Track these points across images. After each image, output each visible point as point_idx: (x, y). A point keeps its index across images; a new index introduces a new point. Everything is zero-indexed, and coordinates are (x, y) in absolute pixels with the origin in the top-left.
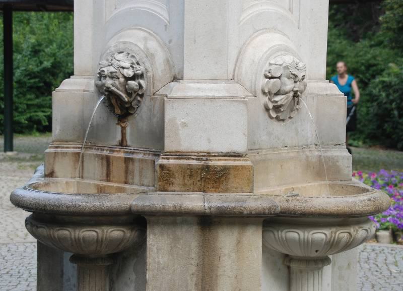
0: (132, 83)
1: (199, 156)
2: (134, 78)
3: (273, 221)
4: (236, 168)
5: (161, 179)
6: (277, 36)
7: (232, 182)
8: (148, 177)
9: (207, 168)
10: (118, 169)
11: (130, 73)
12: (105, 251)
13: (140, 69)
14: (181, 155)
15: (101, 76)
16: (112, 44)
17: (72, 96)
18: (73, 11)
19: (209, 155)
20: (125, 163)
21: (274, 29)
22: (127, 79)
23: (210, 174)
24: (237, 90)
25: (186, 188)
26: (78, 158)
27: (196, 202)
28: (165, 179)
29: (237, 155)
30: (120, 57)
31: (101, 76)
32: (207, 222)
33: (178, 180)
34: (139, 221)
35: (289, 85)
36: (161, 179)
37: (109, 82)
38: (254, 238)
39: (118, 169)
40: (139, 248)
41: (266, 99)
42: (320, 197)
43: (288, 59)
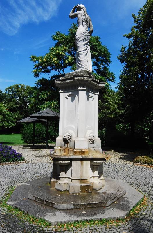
0: (70, 138)
1: (80, 149)
2: (70, 137)
3: (91, 160)
4: (86, 151)
5: (75, 153)
6: (90, 130)
7: (86, 153)
8: (72, 153)
9: (82, 151)
10: (67, 151)
11: (69, 136)
12: (65, 165)
13: (71, 136)
14: (77, 149)
15: (64, 137)
16: (66, 131)
17: (59, 139)
18: (99, 120)
19: (82, 149)
20: (94, 142)
21: (90, 130)
22: (68, 137)
23: (82, 152)
24: (85, 139)
25: (78, 154)
26: (60, 150)
27: (80, 157)
28: (75, 153)
29: (86, 149)
30: (67, 134)
31: (64, 137)
32: (82, 160)
33: (77, 153)
34: (71, 160)
35: (93, 138)
36: (75, 153)
37: (66, 138)
38: (89, 162)
39: (67, 151)
40: (70, 165)
41: (90, 140)
42: (99, 156)
43: (93, 134)
